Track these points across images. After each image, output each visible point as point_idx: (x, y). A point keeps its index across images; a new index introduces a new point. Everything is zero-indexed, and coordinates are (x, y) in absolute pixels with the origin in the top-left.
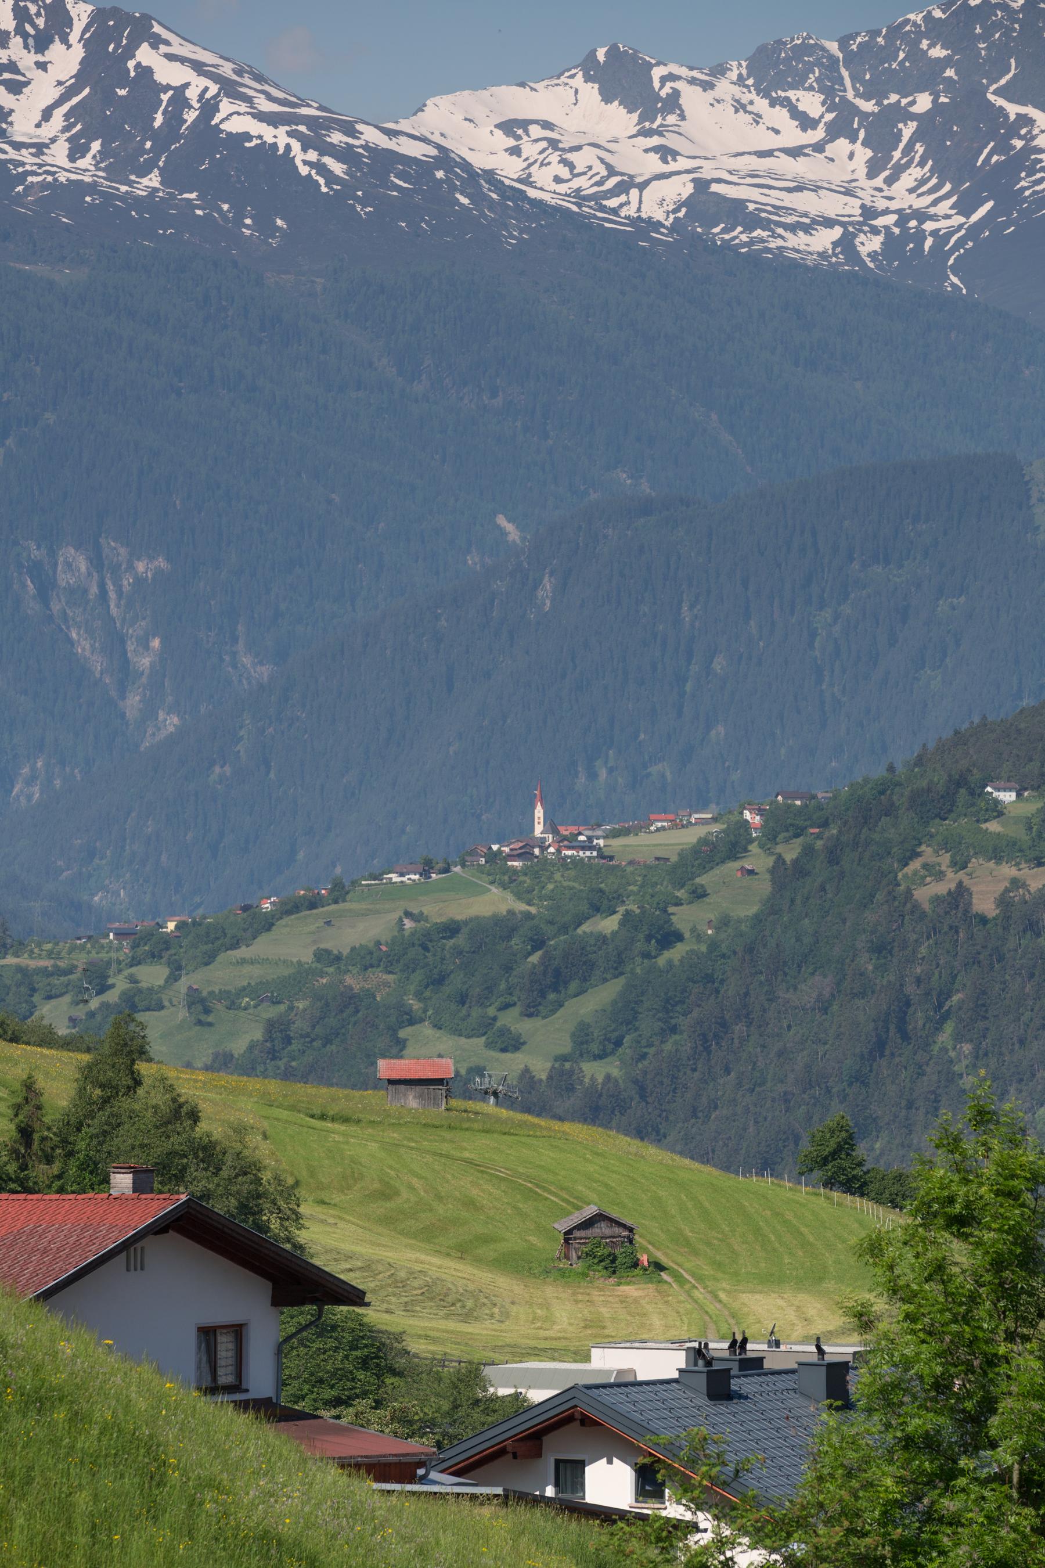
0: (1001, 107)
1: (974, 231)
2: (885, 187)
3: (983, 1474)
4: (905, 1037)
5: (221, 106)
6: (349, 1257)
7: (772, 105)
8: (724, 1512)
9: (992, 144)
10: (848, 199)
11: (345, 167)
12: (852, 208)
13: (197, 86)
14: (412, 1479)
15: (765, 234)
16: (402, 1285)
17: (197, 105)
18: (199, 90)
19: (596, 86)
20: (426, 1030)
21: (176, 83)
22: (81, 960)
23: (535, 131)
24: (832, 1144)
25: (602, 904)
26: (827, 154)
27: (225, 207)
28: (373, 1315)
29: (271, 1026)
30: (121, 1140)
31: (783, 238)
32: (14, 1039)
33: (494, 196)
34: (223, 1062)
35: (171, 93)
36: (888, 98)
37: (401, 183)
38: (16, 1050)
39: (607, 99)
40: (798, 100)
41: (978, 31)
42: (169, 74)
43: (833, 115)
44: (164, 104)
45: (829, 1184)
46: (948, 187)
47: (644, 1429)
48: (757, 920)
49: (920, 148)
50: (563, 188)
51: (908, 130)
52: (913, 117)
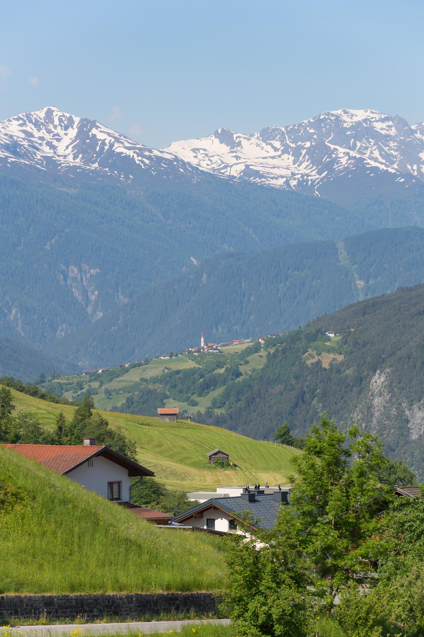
1: (322, 180)
2: (298, 167)
4: (304, 402)
12: (289, 173)
13: (108, 139)
17: (108, 145)
18: (109, 141)
21: (103, 139)
22: (75, 380)
25: (219, 365)
26: (282, 158)
27: (116, 172)
29: (128, 399)
33: (190, 169)
35: (101, 141)
37: (164, 166)
41: (323, 125)
42: (100, 136)
45: (282, 443)
46: (315, 167)
48: (263, 369)
49: (307, 157)
51: (304, 152)
52: (305, 148)
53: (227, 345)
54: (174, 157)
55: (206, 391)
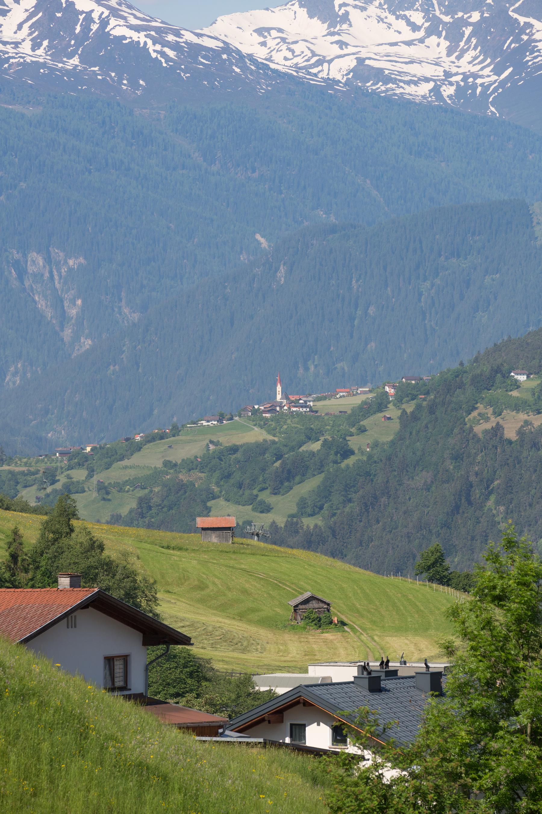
0: (516, 18)
1: (502, 84)
2: (456, 61)
3: (512, 729)
4: (470, 503)
5: (110, 22)
6: (182, 620)
7: (397, 19)
8: (378, 750)
9: (512, 38)
10: (437, 67)
11: (175, 53)
12: (439, 72)
13: (98, 11)
14: (216, 734)
15: (394, 86)
16: (209, 634)
17: (98, 21)
19: (306, 10)
20: (221, 502)
21: (87, 10)
22: (42, 467)
23: (274, 33)
24: (432, 559)
28: (195, 650)
29: (141, 501)
30: (63, 561)
31: (403, 88)
32: (8, 509)
33: (253, 67)
34: (116, 519)
35: (84, 15)
36: (457, 15)
37: (204, 61)
38: (9, 514)
39: (311, 16)
40: (410, 16)
43: (429, 23)
44: (81, 21)
45: (431, 580)
46: (489, 60)
47: (335, 707)
48: (393, 443)
49: (474, 41)
50: (288, 63)
51: (468, 31)
52: (470, 24)
53: (324, 398)
54: (221, 45)
55: (286, 484)
